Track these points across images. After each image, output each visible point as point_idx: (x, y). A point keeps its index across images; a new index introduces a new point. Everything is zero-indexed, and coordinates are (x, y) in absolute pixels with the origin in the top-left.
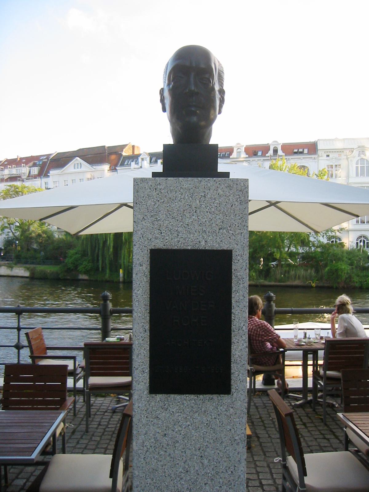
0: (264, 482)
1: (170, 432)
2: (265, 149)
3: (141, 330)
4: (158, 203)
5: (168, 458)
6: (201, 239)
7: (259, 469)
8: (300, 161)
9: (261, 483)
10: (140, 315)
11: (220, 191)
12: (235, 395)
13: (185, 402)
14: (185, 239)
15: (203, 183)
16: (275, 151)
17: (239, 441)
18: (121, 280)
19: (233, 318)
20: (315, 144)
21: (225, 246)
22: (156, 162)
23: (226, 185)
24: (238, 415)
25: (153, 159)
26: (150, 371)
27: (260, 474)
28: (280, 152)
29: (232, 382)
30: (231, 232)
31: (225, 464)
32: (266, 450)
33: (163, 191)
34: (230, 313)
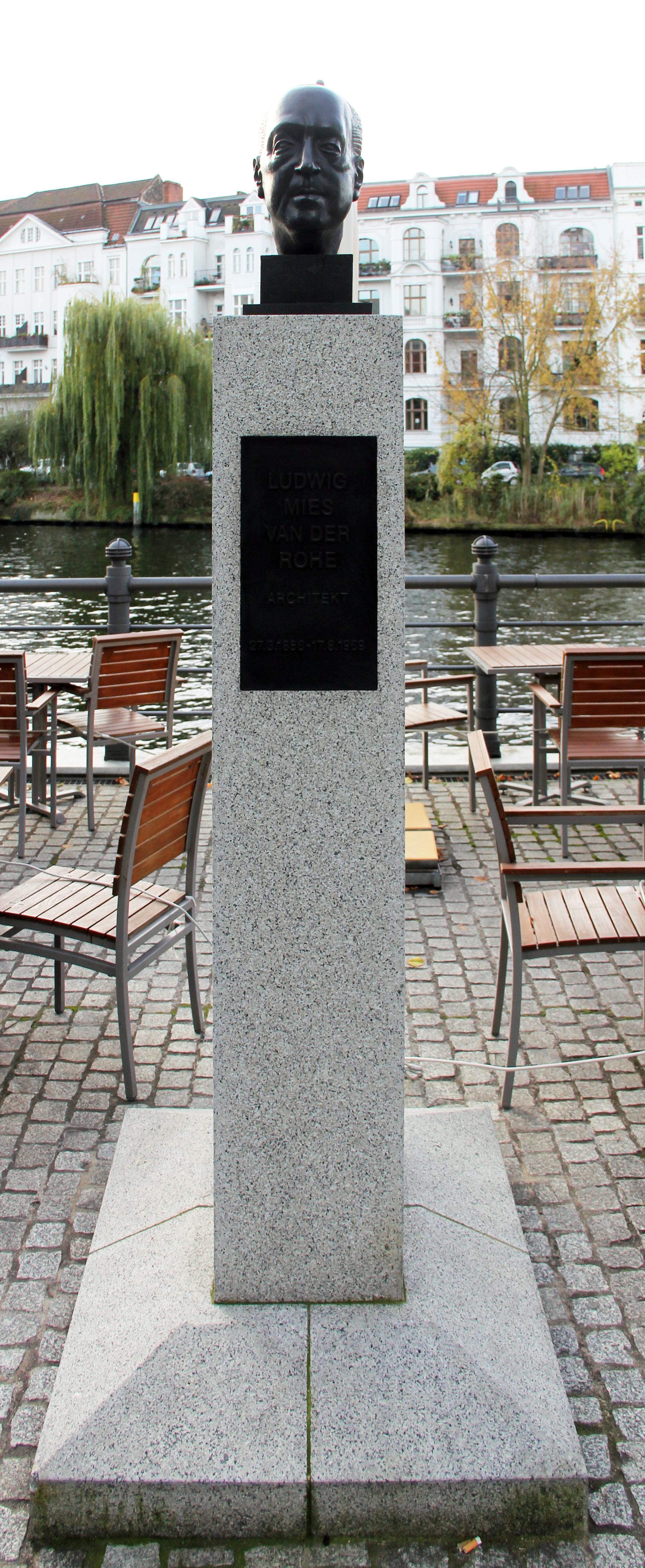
0: (465, 953)
1: (276, 758)
2: (485, 187)
3: (227, 577)
4: (254, 359)
5: (273, 807)
6: (325, 419)
7: (455, 929)
8: (570, 215)
9: (458, 955)
10: (225, 550)
11: (355, 336)
12: (384, 689)
13: (300, 704)
14: (298, 419)
15: (326, 324)
16: (511, 191)
17: (393, 774)
18: (136, 520)
19: (379, 553)
20: (605, 174)
21: (365, 431)
22: (221, 221)
23: (366, 326)
24: (390, 726)
25: (215, 215)
26: (241, 649)
27: (458, 939)
28: (522, 195)
29: (380, 667)
30: (374, 406)
31: (370, 817)
32: (475, 892)
33: (261, 338)
34: (375, 545)
